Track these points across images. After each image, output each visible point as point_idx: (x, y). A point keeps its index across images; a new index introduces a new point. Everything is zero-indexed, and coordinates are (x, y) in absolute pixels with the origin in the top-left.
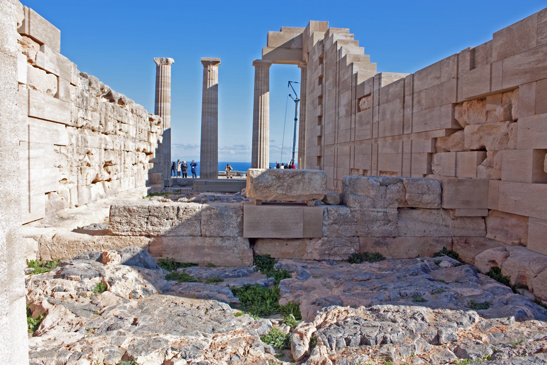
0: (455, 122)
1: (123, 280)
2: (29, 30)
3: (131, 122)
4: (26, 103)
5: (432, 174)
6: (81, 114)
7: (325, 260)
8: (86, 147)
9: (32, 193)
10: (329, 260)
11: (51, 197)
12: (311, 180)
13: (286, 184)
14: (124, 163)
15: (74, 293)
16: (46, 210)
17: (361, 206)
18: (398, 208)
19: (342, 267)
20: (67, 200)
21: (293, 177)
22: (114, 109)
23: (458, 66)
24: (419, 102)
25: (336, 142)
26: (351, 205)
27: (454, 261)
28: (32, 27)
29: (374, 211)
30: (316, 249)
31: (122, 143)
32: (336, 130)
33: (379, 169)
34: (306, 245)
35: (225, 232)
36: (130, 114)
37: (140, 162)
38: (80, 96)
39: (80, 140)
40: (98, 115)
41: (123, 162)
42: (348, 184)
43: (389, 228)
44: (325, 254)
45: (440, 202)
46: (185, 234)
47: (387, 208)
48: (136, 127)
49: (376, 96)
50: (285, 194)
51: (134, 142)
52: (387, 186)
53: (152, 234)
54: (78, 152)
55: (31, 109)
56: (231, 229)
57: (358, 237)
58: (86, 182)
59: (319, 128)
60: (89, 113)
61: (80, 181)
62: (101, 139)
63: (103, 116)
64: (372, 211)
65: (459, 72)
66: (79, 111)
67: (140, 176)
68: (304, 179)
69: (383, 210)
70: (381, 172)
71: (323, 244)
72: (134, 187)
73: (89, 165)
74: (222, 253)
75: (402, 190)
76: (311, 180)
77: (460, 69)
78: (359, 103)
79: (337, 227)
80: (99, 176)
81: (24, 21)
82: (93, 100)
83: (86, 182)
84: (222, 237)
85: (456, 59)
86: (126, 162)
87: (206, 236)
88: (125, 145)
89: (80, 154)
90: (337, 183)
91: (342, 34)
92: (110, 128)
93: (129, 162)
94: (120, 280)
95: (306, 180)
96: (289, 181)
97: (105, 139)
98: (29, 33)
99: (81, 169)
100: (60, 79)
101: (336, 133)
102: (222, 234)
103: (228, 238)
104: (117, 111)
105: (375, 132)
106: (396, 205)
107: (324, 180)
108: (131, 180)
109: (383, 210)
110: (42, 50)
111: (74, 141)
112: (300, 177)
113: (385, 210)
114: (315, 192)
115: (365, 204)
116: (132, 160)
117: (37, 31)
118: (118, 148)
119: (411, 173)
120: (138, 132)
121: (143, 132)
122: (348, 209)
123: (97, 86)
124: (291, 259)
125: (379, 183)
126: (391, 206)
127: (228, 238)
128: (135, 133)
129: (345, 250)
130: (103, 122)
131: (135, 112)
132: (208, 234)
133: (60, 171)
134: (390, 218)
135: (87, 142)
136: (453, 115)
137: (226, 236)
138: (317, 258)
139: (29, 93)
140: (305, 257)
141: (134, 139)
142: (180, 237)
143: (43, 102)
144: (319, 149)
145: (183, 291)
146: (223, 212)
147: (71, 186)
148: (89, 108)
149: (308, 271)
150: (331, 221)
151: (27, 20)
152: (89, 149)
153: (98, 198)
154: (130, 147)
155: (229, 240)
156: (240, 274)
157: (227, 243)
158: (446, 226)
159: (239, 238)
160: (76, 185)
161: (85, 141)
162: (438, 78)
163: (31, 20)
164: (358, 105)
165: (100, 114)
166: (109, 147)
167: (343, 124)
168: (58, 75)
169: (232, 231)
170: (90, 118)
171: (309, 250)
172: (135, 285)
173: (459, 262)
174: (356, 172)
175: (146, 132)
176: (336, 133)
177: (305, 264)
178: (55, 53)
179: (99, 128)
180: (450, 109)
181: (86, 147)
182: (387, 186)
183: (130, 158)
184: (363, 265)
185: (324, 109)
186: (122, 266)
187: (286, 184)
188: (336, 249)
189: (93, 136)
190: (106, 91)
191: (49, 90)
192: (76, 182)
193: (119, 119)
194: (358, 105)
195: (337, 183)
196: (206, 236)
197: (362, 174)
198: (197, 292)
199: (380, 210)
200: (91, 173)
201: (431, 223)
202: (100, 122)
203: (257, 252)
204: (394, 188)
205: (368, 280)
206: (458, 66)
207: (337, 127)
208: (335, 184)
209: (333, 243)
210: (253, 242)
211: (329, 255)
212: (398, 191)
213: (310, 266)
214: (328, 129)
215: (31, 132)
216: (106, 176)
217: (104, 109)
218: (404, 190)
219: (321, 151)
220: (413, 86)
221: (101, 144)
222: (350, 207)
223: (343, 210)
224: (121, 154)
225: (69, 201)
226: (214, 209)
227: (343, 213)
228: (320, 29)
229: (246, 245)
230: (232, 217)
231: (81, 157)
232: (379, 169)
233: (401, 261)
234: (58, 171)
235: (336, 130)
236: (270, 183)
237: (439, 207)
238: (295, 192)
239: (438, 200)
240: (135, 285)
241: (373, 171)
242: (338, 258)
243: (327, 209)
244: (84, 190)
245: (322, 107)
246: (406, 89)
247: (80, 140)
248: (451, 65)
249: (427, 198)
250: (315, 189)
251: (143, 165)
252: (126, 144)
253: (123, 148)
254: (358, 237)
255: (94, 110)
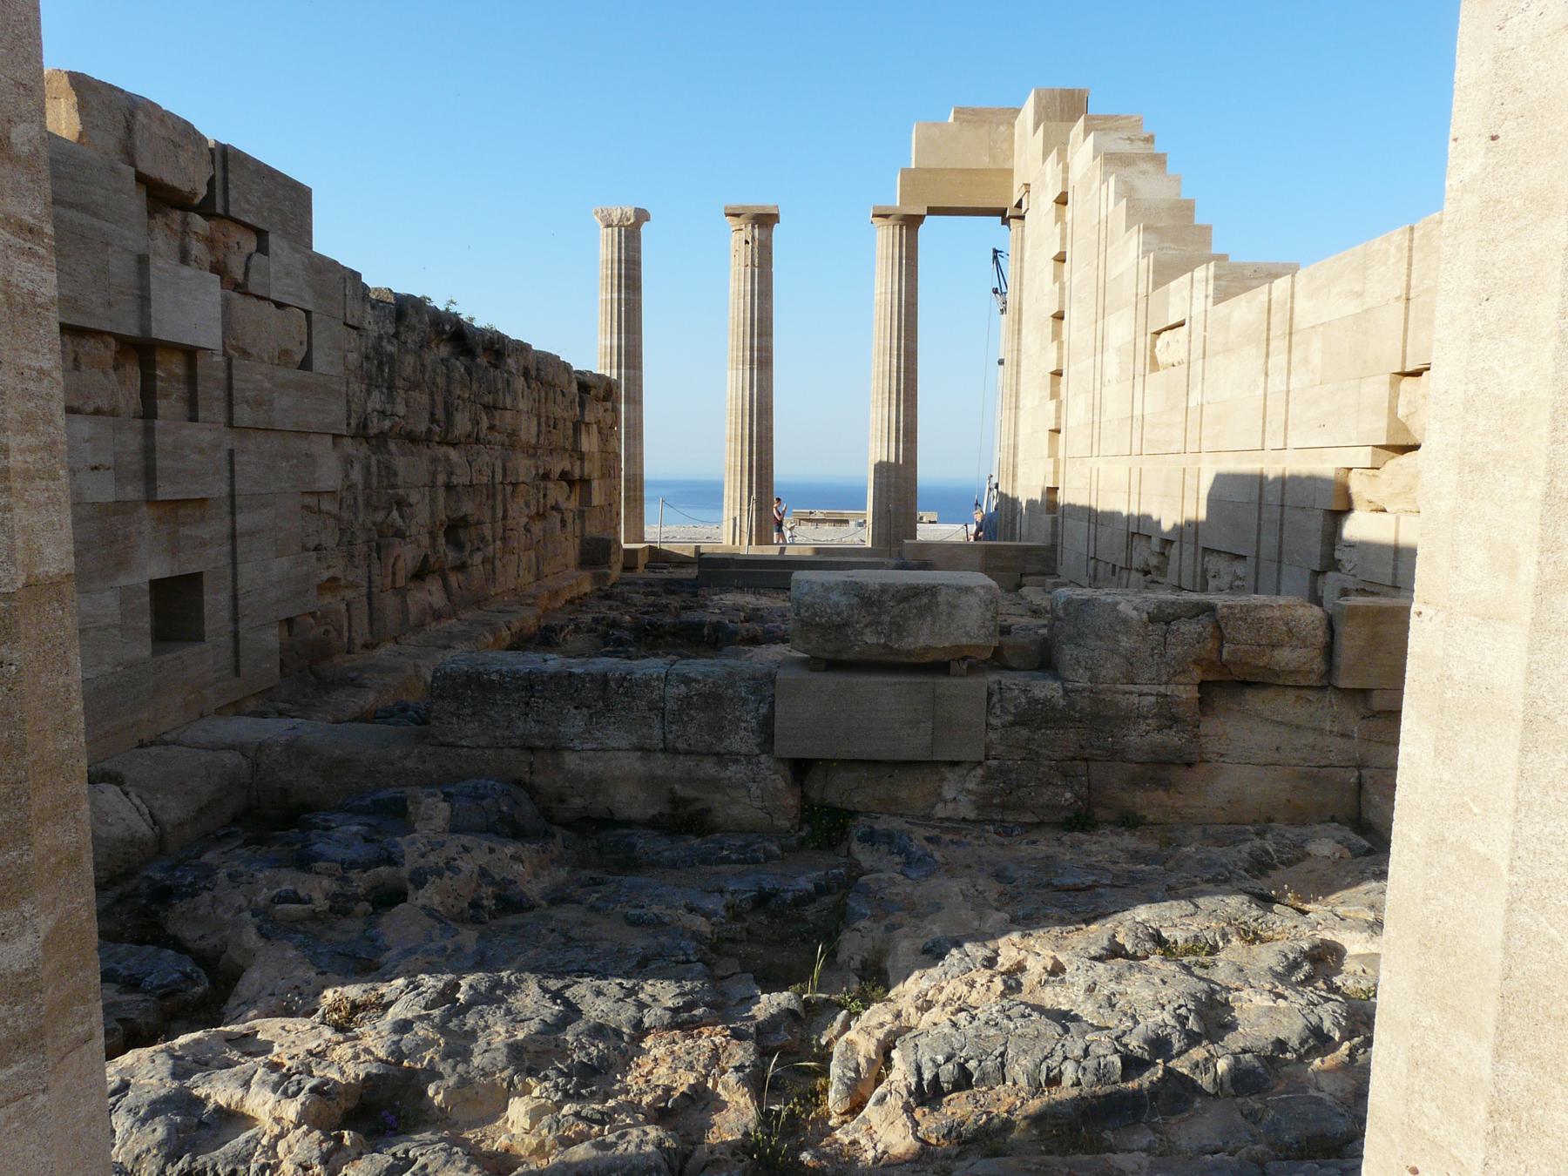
0: (1396, 424)
1: (448, 874)
2: (226, 201)
3: (523, 405)
4: (221, 394)
5: (1339, 570)
6: (376, 401)
7: (992, 822)
8: (393, 487)
9: (242, 626)
10: (1003, 821)
11: (296, 630)
12: (955, 607)
13: (886, 619)
14: (504, 518)
15: (321, 904)
16: (282, 664)
17: (1094, 679)
18: (1202, 686)
19: (1034, 842)
20: (340, 633)
21: (906, 599)
22: (470, 375)
23: (1410, 264)
24: (1306, 360)
25: (1095, 453)
26: (1068, 674)
27: (1355, 839)
28: (233, 195)
29: (1131, 693)
30: (969, 792)
31: (499, 464)
32: (1096, 418)
33: (1201, 543)
34: (943, 779)
35: (727, 742)
36: (520, 383)
37: (553, 508)
38: (372, 354)
39: (374, 470)
40: (425, 398)
41: (500, 515)
42: (1061, 614)
43: (1173, 738)
44: (992, 805)
45: (1323, 668)
46: (624, 744)
47: (1167, 683)
48: (539, 417)
49: (1198, 328)
50: (885, 646)
51: (534, 456)
52: (1168, 623)
53: (538, 743)
54: (367, 505)
55: (236, 409)
56: (742, 733)
57: (1086, 760)
58: (394, 581)
59: (1052, 405)
60: (400, 396)
61: (377, 579)
62: (434, 460)
63: (439, 399)
64: (1125, 693)
65: (1413, 282)
66: (369, 392)
67: (550, 547)
68: (937, 604)
69: (1155, 689)
70: (1205, 549)
71: (985, 780)
72: (531, 579)
73: (400, 534)
74: (718, 796)
75: (1213, 636)
76: (955, 607)
77: (1414, 276)
78: (1154, 346)
79: (1025, 732)
80: (432, 560)
81: (211, 183)
82: (410, 360)
83: (394, 581)
84: (718, 754)
85: (1406, 243)
86: (510, 513)
87: (676, 752)
88: (504, 469)
89: (376, 509)
90: (1096, 569)
91: (1119, 134)
92: (462, 423)
93: (519, 511)
94: (440, 875)
95: (943, 608)
96: (896, 611)
97: (447, 459)
98: (226, 209)
99: (379, 548)
100: (315, 317)
101: (1096, 426)
102: (719, 748)
103: (735, 758)
104: (479, 380)
105: (1193, 435)
106: (1197, 675)
107: (991, 607)
108: (524, 559)
109: (1155, 689)
110: (263, 248)
111: (356, 475)
112: (925, 600)
113: (1162, 689)
114: (964, 641)
115: (1104, 672)
116: (527, 505)
117: (247, 200)
118: (485, 480)
119: (1280, 562)
120: (543, 429)
121: (560, 426)
122: (1056, 685)
123: (421, 321)
124: (902, 816)
125: (1145, 616)
126: (1181, 679)
127: (735, 758)
128: (534, 430)
129: (1047, 794)
130: (440, 415)
131: (534, 373)
132: (681, 745)
133: (319, 559)
134: (1179, 711)
135: (395, 475)
136: (1393, 410)
137: (731, 753)
138: (972, 815)
139: (229, 367)
140: (940, 811)
141: (532, 451)
142: (610, 754)
143: (268, 385)
144: (1051, 468)
145: (600, 904)
146: (720, 691)
147: (350, 594)
148: (399, 383)
149: (937, 855)
150: (1011, 718)
151: (219, 175)
152: (401, 492)
153: (429, 619)
154: (522, 471)
155: (736, 762)
156: (761, 855)
157: (732, 772)
158: (1343, 735)
159: (763, 758)
160: (364, 590)
161: (389, 471)
162: (1359, 295)
163: (230, 176)
164: (1152, 351)
165: (432, 395)
166: (460, 479)
167: (1115, 404)
168: (309, 307)
169: (742, 740)
170: (401, 409)
171: (949, 793)
172: (480, 886)
173: (1367, 845)
174: (1143, 542)
175: (569, 424)
176: (1096, 426)
177: (937, 832)
178: (298, 251)
179: (429, 431)
180: (1385, 389)
181: (393, 487)
182: (1168, 623)
183: (522, 503)
184: (1095, 838)
185: (1065, 352)
186: (447, 836)
187: (886, 619)
188: (1022, 793)
189: (413, 454)
190: (447, 327)
191: (285, 353)
192: (365, 584)
193: (488, 399)
194: (1152, 351)
195: (1096, 569)
196: (676, 752)
197: (1157, 549)
198: (636, 907)
199: (1145, 689)
200: (407, 555)
201: (1298, 727)
202: (432, 414)
203: (814, 794)
204: (1188, 628)
205: (1090, 887)
206: (1410, 264)
207: (1097, 406)
208: (1091, 572)
209: (1013, 776)
210: (800, 768)
211: (1004, 807)
212: (1200, 639)
213: (947, 838)
214: (1076, 415)
215: (237, 468)
216: (452, 556)
217: (440, 380)
218: (1220, 637)
219: (1056, 473)
220: (1292, 309)
221: (434, 475)
222: (1064, 680)
223: (1047, 689)
224: (494, 496)
225: (346, 635)
226: (698, 682)
227: (1042, 695)
228: (1062, 110)
229: (779, 781)
230: (745, 701)
231: (380, 516)
232: (1201, 543)
233: (1204, 831)
234: (314, 560)
235: (1096, 418)
236: (845, 615)
237: (1325, 682)
238: (911, 640)
239: (1318, 665)
240: (480, 886)
241: (1185, 546)
242: (1028, 818)
243: (1000, 683)
244: (389, 602)
245: (1060, 348)
246: (1275, 319)
247: (374, 470)
248: (1392, 260)
249: (1286, 657)
250: (967, 634)
251: (559, 517)
252: (509, 464)
253: (499, 478)
254: (1086, 760)
255: (416, 386)
